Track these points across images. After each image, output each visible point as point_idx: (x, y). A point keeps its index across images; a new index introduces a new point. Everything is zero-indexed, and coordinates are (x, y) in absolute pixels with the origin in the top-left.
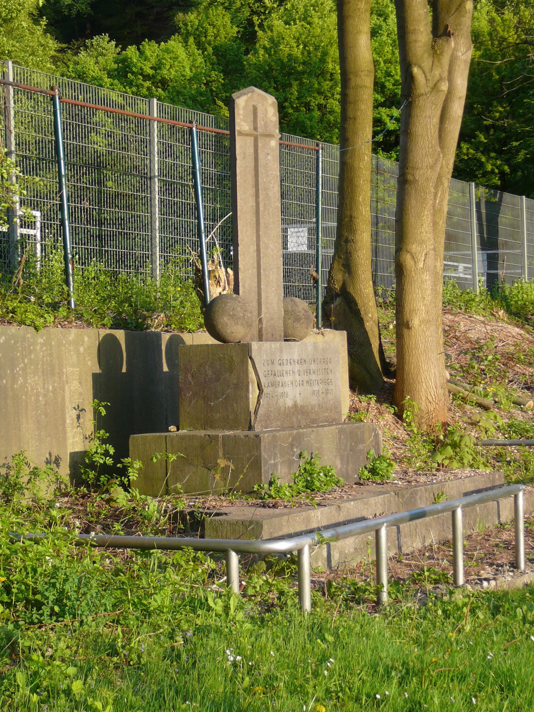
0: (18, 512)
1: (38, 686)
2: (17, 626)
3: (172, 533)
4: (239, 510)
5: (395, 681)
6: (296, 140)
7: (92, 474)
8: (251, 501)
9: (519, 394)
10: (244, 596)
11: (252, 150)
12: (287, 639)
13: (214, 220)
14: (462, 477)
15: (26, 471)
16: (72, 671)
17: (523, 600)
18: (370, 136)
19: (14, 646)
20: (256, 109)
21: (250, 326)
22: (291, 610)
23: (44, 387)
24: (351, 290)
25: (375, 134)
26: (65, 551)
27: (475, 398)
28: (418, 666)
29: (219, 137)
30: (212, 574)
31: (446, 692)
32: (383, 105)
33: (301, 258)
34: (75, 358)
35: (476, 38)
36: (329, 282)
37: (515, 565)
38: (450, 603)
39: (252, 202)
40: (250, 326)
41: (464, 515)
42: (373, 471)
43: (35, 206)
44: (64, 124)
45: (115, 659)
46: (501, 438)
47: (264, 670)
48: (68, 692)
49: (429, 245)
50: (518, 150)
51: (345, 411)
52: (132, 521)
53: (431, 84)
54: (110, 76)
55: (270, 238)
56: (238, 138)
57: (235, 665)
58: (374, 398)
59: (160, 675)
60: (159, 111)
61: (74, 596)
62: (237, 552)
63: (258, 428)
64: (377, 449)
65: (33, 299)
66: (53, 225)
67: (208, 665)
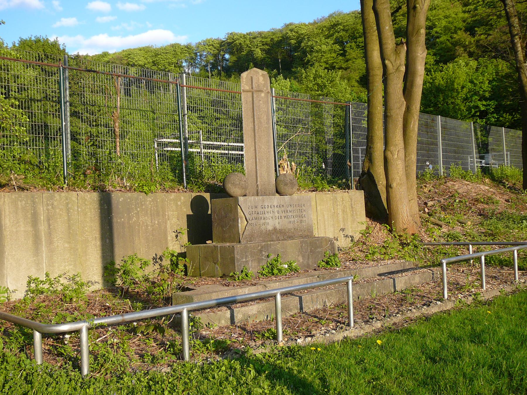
11: (251, 99)
23: (152, 222)
24: (371, 171)
28: (438, 345)
34: (174, 207)
39: (251, 125)
44: (125, 90)
53: (395, 68)
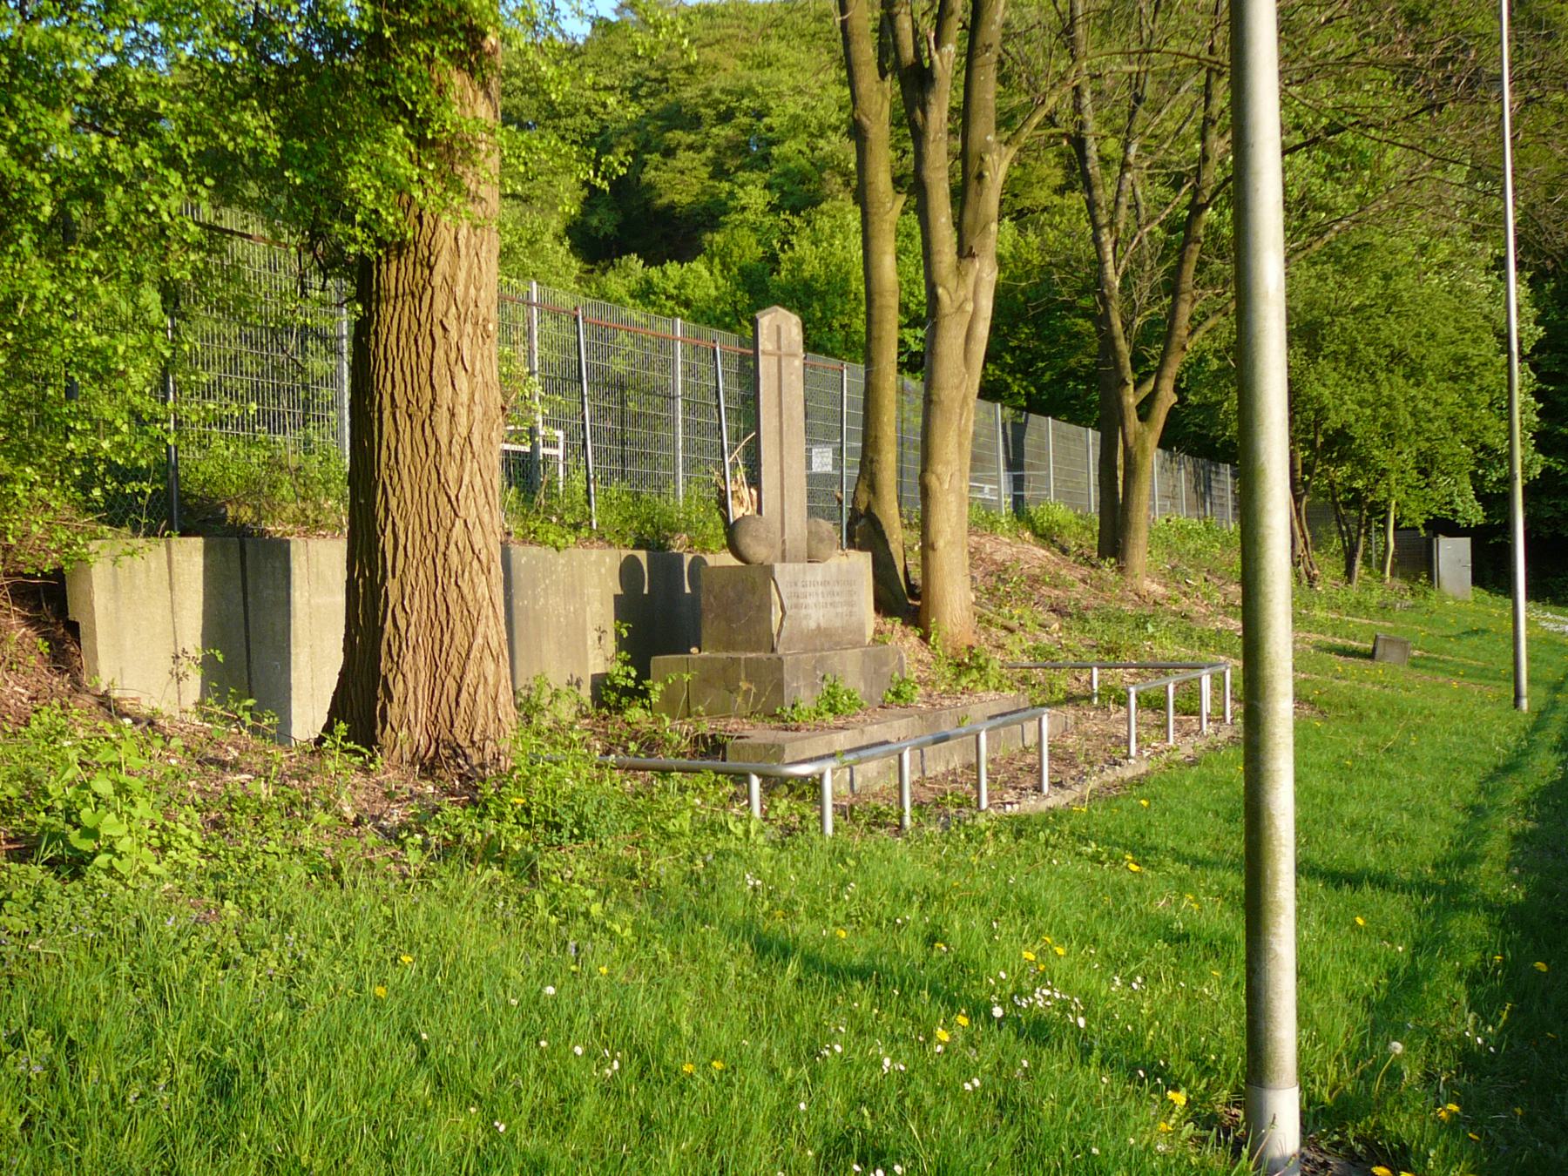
0: (538, 734)
1: (556, 908)
2: (536, 848)
3: (693, 755)
4: (760, 733)
5: (917, 905)
6: (820, 360)
7: (613, 696)
8: (774, 724)
9: (1045, 616)
10: (765, 819)
12: (807, 864)
13: (737, 440)
14: (986, 701)
15: (547, 692)
16: (590, 893)
17: (1046, 824)
18: (895, 356)
19: (533, 868)
20: (780, 329)
21: (773, 547)
22: (813, 834)
24: (875, 511)
25: (900, 354)
26: (584, 774)
27: (1000, 620)
28: (939, 891)
29: (743, 357)
30: (734, 797)
31: (968, 916)
32: (908, 326)
33: (825, 478)
34: (596, 580)
35: (1000, 260)
36: (853, 502)
37: (1038, 789)
38: (972, 827)
39: (775, 422)
40: (773, 547)
41: (988, 738)
42: (897, 694)
43: (558, 426)
45: (634, 882)
46: (1026, 661)
47: (784, 894)
48: (586, 915)
49: (955, 466)
50: (1044, 371)
51: (869, 633)
52: (650, 744)
53: (956, 304)
54: (632, 296)
55: (794, 459)
56: (761, 357)
57: (755, 889)
58: (899, 621)
59: (679, 899)
60: (683, 331)
61: (592, 818)
62: (759, 776)
63: (780, 651)
64: (902, 673)
65: (554, 519)
66: (576, 448)
67: (728, 889)
